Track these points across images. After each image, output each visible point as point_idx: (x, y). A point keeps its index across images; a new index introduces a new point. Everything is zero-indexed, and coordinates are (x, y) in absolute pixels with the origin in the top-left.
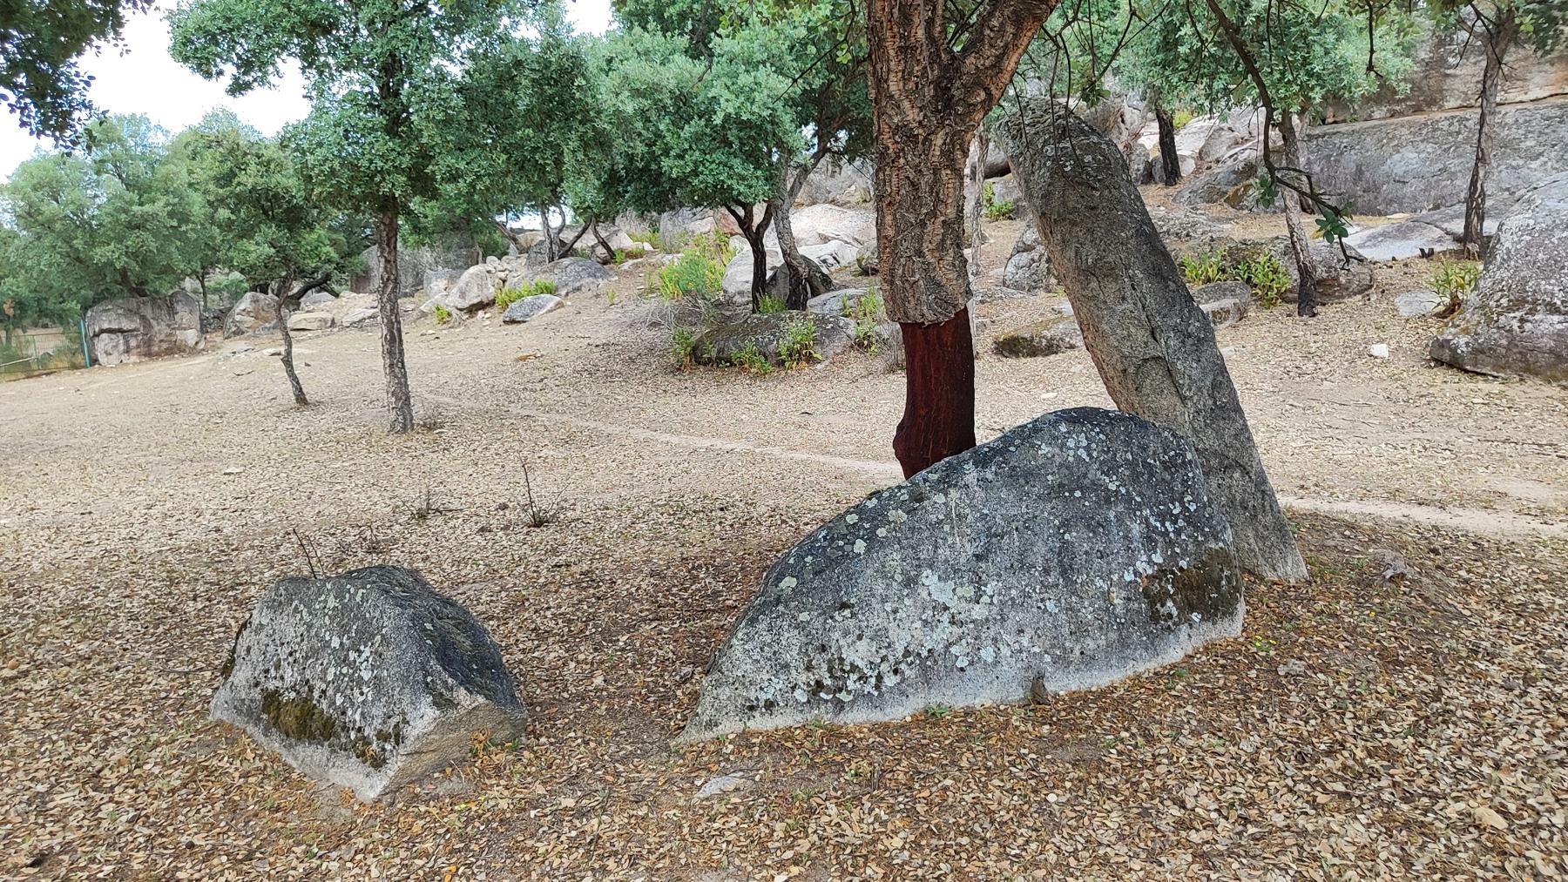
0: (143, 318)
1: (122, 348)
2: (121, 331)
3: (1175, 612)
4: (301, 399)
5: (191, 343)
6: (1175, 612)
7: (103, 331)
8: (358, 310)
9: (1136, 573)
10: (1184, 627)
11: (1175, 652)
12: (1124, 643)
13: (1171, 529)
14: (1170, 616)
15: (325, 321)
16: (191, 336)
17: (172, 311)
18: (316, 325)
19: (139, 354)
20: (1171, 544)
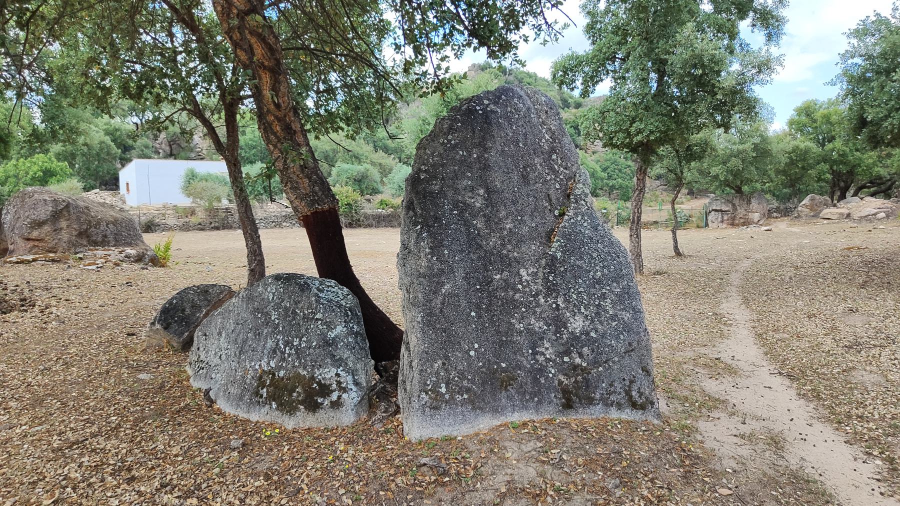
0: (734, 205)
1: (720, 219)
2: (721, 211)
3: (265, 395)
4: (678, 253)
5: (756, 220)
6: (265, 395)
7: (713, 210)
8: (869, 209)
9: (260, 365)
10: (267, 407)
11: (256, 416)
12: (241, 399)
13: (287, 352)
14: (261, 396)
15: (842, 214)
16: (756, 216)
17: (749, 202)
18: (836, 216)
19: (728, 224)
20: (284, 359)
